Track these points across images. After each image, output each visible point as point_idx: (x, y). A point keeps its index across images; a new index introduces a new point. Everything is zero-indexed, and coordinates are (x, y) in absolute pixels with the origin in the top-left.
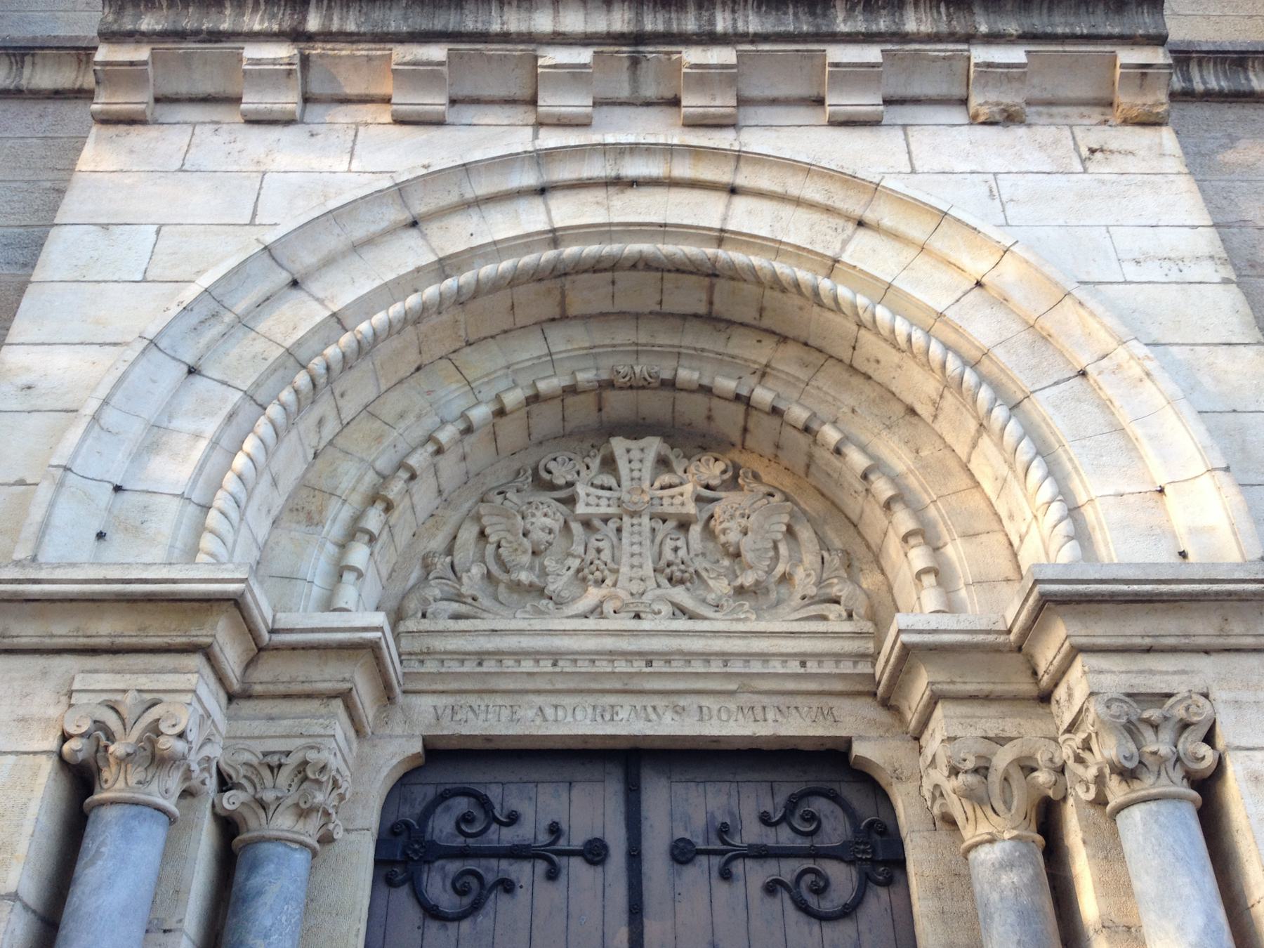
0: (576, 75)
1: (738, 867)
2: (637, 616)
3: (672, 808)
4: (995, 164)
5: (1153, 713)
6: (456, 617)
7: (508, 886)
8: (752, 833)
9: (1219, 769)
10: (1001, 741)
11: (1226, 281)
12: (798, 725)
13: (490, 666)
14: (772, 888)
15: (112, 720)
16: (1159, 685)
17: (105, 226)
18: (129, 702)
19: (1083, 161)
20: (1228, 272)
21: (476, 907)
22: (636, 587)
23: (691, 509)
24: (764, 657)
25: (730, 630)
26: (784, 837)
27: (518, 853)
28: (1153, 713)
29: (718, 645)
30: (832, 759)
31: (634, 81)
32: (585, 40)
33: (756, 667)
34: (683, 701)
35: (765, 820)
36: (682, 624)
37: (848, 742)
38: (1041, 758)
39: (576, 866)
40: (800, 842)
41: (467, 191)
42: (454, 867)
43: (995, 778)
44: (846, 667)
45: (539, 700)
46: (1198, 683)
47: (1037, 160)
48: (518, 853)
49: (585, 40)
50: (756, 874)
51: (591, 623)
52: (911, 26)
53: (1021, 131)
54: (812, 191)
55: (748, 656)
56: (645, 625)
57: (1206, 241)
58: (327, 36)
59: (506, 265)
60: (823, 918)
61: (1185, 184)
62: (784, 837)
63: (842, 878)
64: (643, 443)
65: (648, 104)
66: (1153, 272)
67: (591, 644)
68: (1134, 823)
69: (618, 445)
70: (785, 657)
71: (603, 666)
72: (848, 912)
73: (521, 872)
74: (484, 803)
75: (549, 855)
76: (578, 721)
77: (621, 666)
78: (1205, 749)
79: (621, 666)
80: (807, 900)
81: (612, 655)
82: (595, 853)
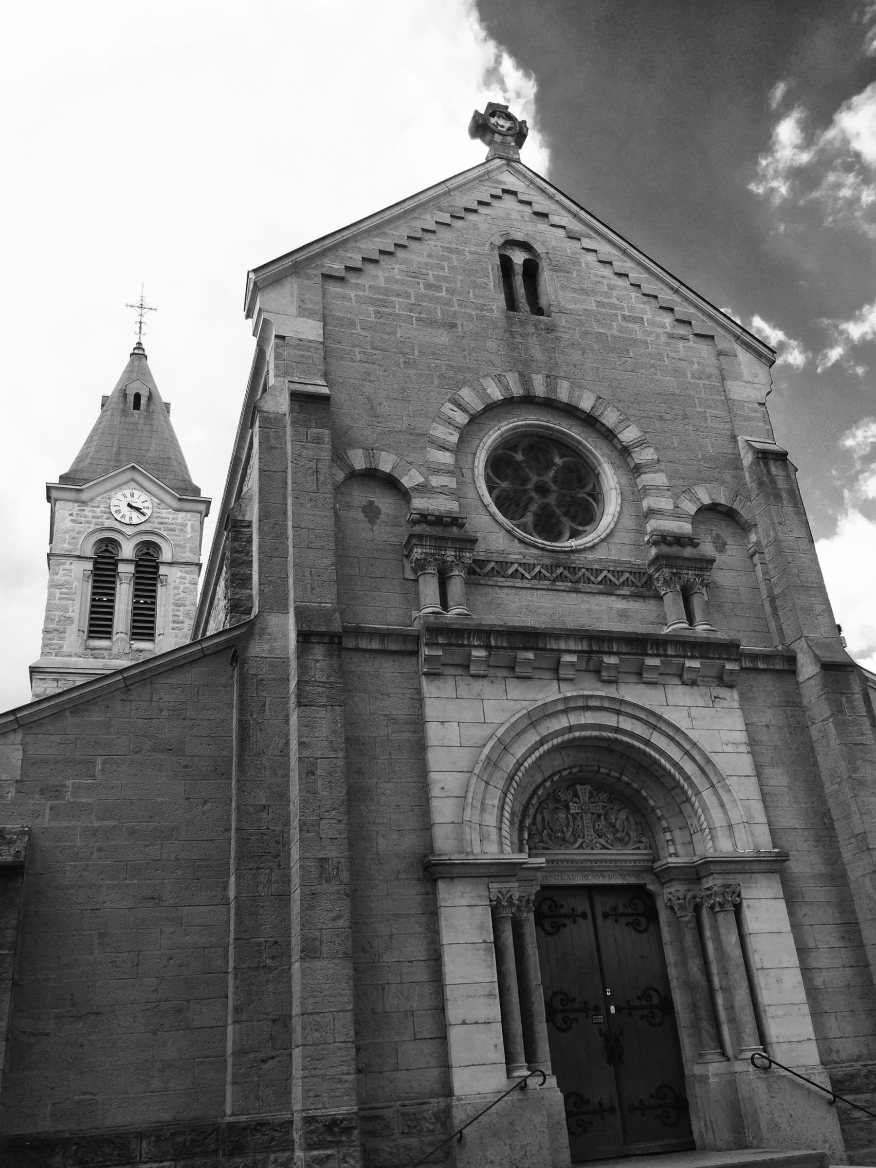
0: (572, 664)
1: (619, 919)
2: (592, 849)
3: (602, 904)
4: (689, 703)
5: (728, 890)
6: (544, 848)
7: (564, 925)
8: (621, 909)
9: (740, 904)
10: (689, 891)
11: (748, 752)
12: (632, 881)
13: (555, 864)
14: (627, 924)
15: (500, 896)
16: (730, 883)
17: (442, 722)
18: (504, 891)
19: (713, 702)
20: (749, 749)
21: (557, 931)
22: (590, 838)
23: (601, 811)
24: (625, 861)
25: (617, 853)
26: (629, 911)
27: (565, 916)
28: (728, 890)
29: (614, 857)
30: (641, 888)
31: (587, 664)
32: (575, 652)
33: (623, 864)
34: (605, 873)
35: (624, 906)
36: (604, 851)
37: (645, 884)
38: (698, 895)
39: (580, 920)
40: (633, 912)
41: (545, 713)
42: (550, 920)
43: (687, 899)
44: (646, 864)
45: (568, 873)
46: (736, 882)
47: (700, 702)
48: (565, 916)
49: (575, 652)
50: (623, 920)
51: (581, 851)
52: (669, 652)
53: (696, 688)
54: (643, 715)
55: (621, 861)
56: (595, 852)
57: (742, 737)
58: (497, 647)
59: (560, 740)
60: (640, 932)
61: (809, 1019)
62: (629, 910)
63: (643, 921)
64: (585, 787)
65: (590, 671)
66: (730, 748)
67: (582, 857)
68: (721, 917)
69: (579, 787)
70: (630, 861)
71: (584, 864)
72: (645, 930)
73: (567, 921)
74: (554, 901)
75: (573, 916)
76: (580, 880)
77: (589, 864)
78: (738, 899)
79: (589, 864)
80: (635, 926)
81: (587, 861)
82: (584, 916)
